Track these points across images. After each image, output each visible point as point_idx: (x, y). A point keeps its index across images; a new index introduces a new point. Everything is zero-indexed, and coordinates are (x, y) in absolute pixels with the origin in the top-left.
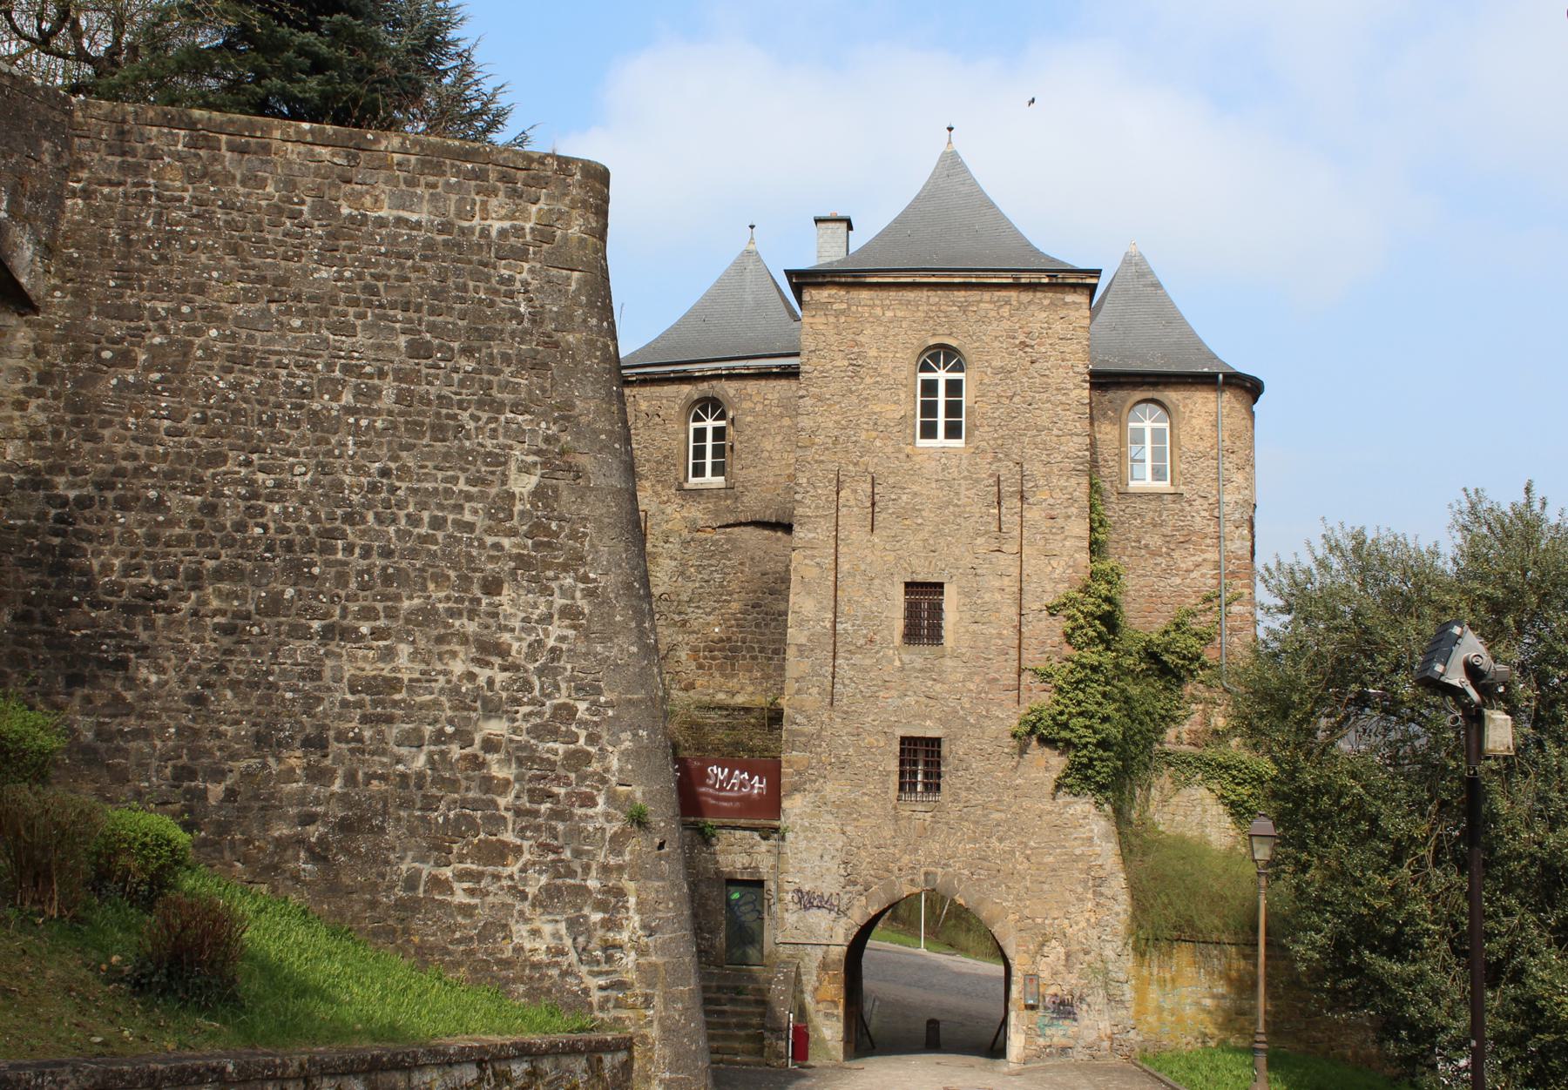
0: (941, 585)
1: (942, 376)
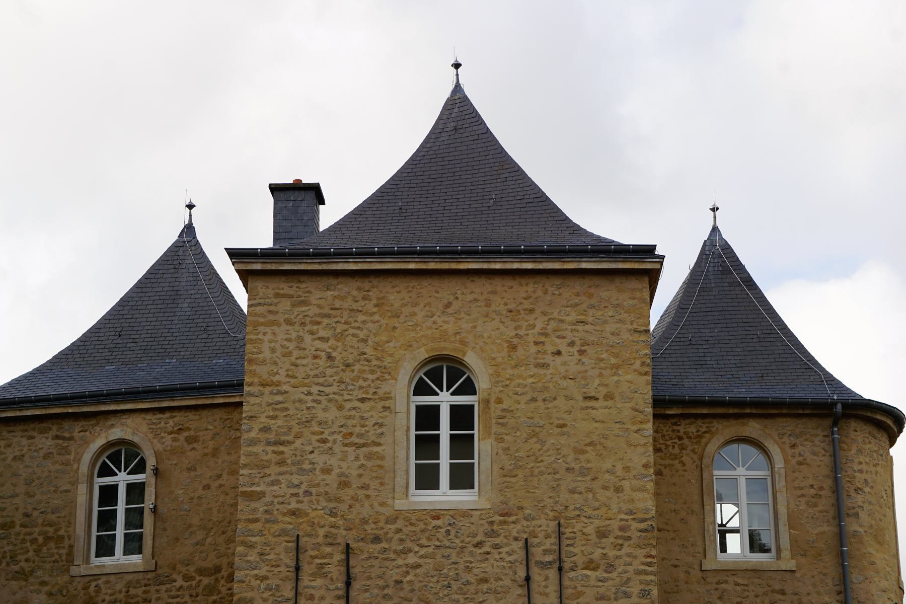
1: (122, 479)
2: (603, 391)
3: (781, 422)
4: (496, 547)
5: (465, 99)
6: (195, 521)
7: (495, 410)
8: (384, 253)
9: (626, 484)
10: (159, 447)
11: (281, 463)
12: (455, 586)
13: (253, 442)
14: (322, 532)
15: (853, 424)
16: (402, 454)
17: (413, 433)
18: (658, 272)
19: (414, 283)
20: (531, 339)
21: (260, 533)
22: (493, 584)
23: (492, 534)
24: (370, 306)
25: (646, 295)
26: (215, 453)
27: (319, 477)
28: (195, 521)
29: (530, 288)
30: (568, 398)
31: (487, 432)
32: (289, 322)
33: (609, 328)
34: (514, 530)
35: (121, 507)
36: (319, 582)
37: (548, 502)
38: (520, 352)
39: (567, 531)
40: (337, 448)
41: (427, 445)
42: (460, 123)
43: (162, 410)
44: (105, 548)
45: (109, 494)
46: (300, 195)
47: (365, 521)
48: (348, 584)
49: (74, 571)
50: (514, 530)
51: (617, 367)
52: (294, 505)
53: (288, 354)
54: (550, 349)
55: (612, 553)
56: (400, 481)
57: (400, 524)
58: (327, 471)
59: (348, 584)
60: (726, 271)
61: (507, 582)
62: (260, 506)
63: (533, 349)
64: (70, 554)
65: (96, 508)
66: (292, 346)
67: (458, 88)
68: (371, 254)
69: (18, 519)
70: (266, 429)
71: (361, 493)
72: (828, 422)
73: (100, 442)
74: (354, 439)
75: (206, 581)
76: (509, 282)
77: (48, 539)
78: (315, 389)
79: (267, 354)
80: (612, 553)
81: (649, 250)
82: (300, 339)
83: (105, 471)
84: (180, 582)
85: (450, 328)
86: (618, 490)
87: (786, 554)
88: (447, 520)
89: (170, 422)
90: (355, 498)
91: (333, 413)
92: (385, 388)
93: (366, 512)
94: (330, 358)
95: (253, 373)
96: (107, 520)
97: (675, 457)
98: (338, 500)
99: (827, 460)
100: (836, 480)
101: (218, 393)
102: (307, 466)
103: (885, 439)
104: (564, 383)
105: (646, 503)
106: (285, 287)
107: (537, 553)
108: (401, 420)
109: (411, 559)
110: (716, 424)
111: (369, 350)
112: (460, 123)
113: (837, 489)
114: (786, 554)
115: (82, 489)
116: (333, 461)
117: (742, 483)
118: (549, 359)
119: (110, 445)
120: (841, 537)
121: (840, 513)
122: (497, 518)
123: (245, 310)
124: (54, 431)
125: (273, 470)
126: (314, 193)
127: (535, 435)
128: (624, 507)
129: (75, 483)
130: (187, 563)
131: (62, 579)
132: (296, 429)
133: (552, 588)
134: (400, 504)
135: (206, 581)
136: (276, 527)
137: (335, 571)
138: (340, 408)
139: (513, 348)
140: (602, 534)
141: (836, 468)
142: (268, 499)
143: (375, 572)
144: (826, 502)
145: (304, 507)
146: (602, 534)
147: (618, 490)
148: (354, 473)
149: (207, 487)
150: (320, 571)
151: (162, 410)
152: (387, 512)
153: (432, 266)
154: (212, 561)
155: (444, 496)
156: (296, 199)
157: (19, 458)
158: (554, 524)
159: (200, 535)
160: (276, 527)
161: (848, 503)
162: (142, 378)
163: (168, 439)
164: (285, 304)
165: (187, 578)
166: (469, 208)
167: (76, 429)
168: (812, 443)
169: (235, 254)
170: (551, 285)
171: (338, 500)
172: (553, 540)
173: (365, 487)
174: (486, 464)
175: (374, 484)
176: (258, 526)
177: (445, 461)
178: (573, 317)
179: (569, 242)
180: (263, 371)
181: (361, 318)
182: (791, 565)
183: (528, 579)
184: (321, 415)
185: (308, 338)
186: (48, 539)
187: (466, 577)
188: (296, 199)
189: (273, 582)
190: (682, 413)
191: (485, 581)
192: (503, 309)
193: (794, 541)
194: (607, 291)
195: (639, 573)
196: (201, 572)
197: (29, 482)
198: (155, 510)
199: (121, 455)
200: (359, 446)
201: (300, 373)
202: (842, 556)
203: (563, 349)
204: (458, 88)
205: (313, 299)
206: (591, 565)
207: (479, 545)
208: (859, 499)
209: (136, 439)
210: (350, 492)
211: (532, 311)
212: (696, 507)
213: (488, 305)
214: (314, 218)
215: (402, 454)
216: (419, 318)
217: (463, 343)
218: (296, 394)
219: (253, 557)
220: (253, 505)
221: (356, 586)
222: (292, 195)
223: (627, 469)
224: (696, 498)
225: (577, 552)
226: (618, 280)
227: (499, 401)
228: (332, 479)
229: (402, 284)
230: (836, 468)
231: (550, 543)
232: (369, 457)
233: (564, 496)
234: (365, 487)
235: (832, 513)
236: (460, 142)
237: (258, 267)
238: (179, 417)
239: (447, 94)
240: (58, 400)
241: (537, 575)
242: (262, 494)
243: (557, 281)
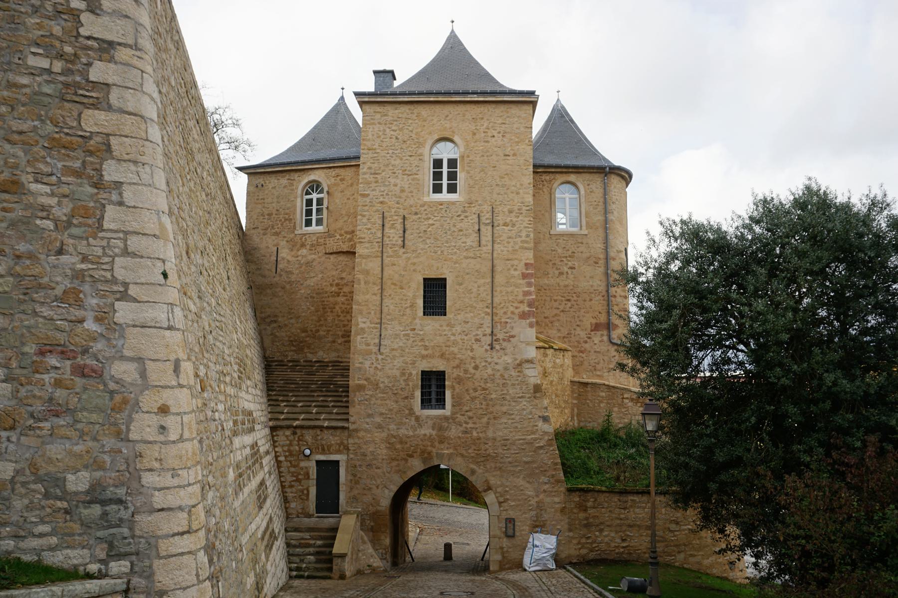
0: (445, 279)
2: (512, 152)
3: (584, 175)
4: (466, 217)
5: (456, 36)
6: (344, 212)
7: (466, 160)
8: (420, 93)
9: (521, 191)
10: (329, 183)
11: (376, 182)
12: (449, 233)
13: (365, 174)
14: (393, 210)
15: (613, 176)
16: (427, 178)
17: (432, 170)
18: (536, 102)
19: (432, 106)
20: (482, 130)
21: (368, 211)
22: (465, 232)
23: (464, 211)
24: (414, 117)
25: (531, 112)
26: (352, 185)
27: (392, 188)
28: (344, 212)
29: (482, 109)
30: (497, 155)
31: (463, 170)
32: (379, 123)
33: (515, 126)
34: (474, 210)
35: (314, 207)
36: (392, 231)
37: (488, 198)
38: (477, 136)
39: (496, 210)
40: (400, 176)
41: (438, 176)
42: (454, 46)
43: (330, 168)
44: (308, 223)
45: (309, 202)
46: (386, 75)
47: (411, 206)
48: (404, 232)
49: (296, 232)
50: (474, 210)
51: (518, 142)
52: (381, 199)
53: (379, 137)
54: (490, 134)
55: (514, 219)
56: (426, 189)
57: (426, 207)
58: (396, 185)
59: (404, 232)
60: (563, 116)
61: (470, 231)
62: (368, 200)
63: (483, 135)
64: (295, 226)
65: (304, 208)
66: (381, 133)
67: (453, 31)
68: (415, 94)
69: (274, 212)
70: (370, 168)
71: (410, 195)
72: (603, 175)
73: (306, 181)
74: (407, 172)
75: (348, 236)
76: (473, 106)
77: (286, 220)
78: (390, 152)
79: (370, 136)
80: (514, 219)
81: (532, 93)
82: (384, 130)
83: (308, 193)
84: (338, 237)
85: (448, 126)
86: (518, 193)
87: (584, 228)
88: (446, 205)
89: (333, 172)
90: (407, 197)
91: (398, 162)
92: (420, 151)
93: (412, 202)
94: (397, 138)
95: (365, 145)
96: (309, 213)
97: (540, 189)
98: (400, 197)
99: (602, 190)
100: (605, 199)
101: (351, 162)
102: (387, 183)
103: (624, 183)
104: (496, 149)
105: (529, 199)
106: (377, 108)
107: (483, 219)
108: (426, 164)
109: (431, 222)
110: (558, 176)
111: (414, 136)
112: (454, 46)
113: (605, 203)
114: (584, 228)
115: (299, 200)
116: (398, 181)
117: (567, 200)
118: (489, 139)
119: (310, 182)
120: (606, 221)
121: (606, 212)
122: (467, 205)
123: (360, 123)
124: (287, 177)
125: (373, 185)
126: (391, 73)
127: (483, 170)
128: (520, 201)
129: (296, 198)
130: (341, 229)
131: (292, 236)
132: (383, 168)
133: (489, 234)
134: (426, 199)
135: (348, 236)
136: (374, 208)
137: (399, 226)
138: (401, 159)
139: (474, 134)
140: (510, 212)
141: (605, 194)
142: (371, 196)
143: (415, 227)
144: (601, 207)
145: (386, 200)
146: (510, 212)
147: (518, 193)
148: (407, 186)
149: (348, 199)
150: (393, 226)
151: (330, 168)
152: (420, 202)
153: (440, 99)
154: (350, 228)
155: (445, 196)
156: (385, 75)
157: (274, 188)
158: (490, 208)
159: (346, 218)
160: (374, 208)
161: (609, 208)
162: (322, 155)
163: (333, 180)
164: (378, 116)
165: (341, 235)
166: (456, 86)
167: (295, 176)
168: (596, 182)
169: (357, 94)
170: (491, 107)
171: (400, 197)
172: (490, 214)
173: (411, 192)
174: (462, 183)
175: (415, 191)
176: (366, 208)
177: (445, 182)
178: (500, 121)
179: (498, 89)
180: (369, 144)
181: (410, 121)
182: (586, 232)
183: (479, 230)
184: (393, 162)
185: (388, 130)
186: (286, 220)
187: (453, 229)
188: (385, 75)
189: (373, 231)
190: (543, 171)
191: (461, 231)
192: (470, 118)
193: (587, 223)
194: (514, 110)
195: (526, 227)
196: (346, 233)
197: (278, 197)
198: (327, 208)
199: (315, 186)
200: (409, 175)
201: (384, 145)
202: (606, 228)
203: (496, 135)
204: (453, 31)
205: (390, 114)
206: (506, 224)
207: (458, 216)
208: (614, 206)
209: (320, 180)
210: (405, 194)
211: (482, 118)
212: (548, 209)
213: (464, 116)
214: (392, 84)
215: (427, 178)
216: (435, 121)
217: (453, 132)
218: (383, 153)
219: (365, 220)
220: (365, 199)
221: (407, 232)
222: (382, 75)
223: (521, 185)
224: (548, 205)
225: (500, 219)
226: (519, 105)
227: (468, 157)
228: (397, 189)
229: (427, 107)
230: (605, 194)
231: (489, 215)
232: (413, 180)
233: (495, 196)
234: (411, 192)
235: (603, 212)
236: (454, 52)
237: (366, 99)
238: (337, 171)
239: (448, 34)
240: (289, 164)
241: (483, 228)
242: (368, 195)
243: (494, 106)
